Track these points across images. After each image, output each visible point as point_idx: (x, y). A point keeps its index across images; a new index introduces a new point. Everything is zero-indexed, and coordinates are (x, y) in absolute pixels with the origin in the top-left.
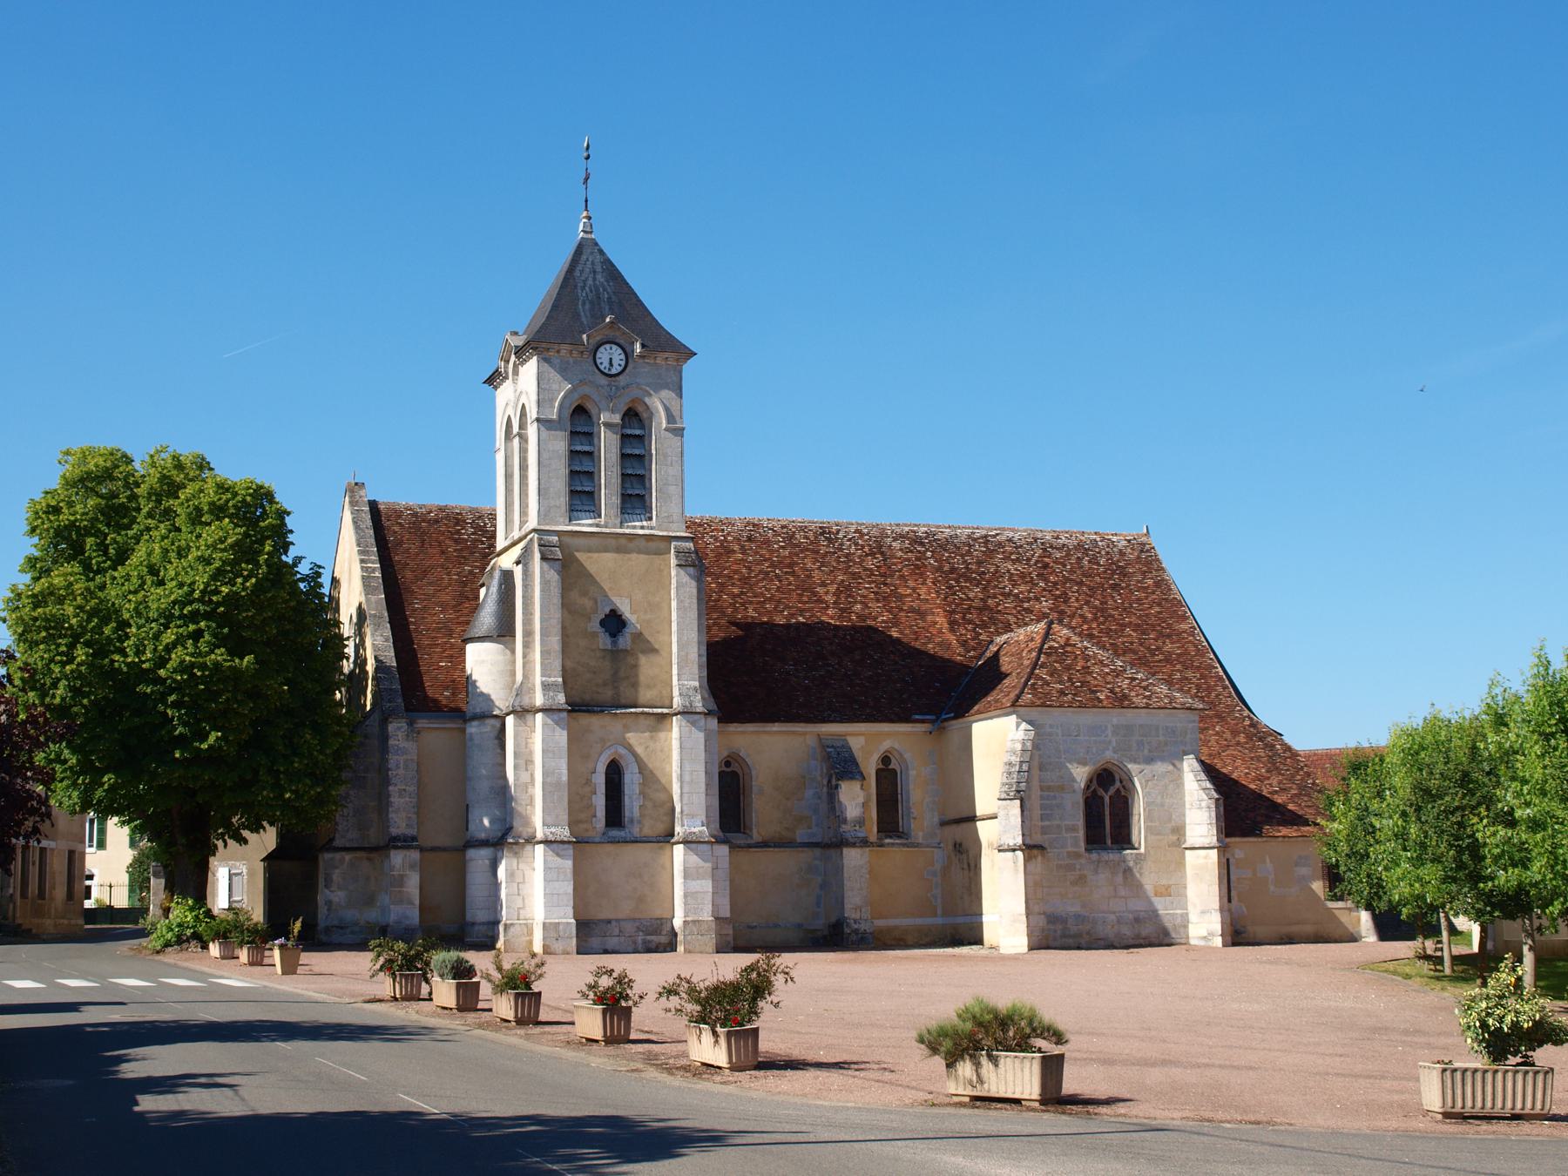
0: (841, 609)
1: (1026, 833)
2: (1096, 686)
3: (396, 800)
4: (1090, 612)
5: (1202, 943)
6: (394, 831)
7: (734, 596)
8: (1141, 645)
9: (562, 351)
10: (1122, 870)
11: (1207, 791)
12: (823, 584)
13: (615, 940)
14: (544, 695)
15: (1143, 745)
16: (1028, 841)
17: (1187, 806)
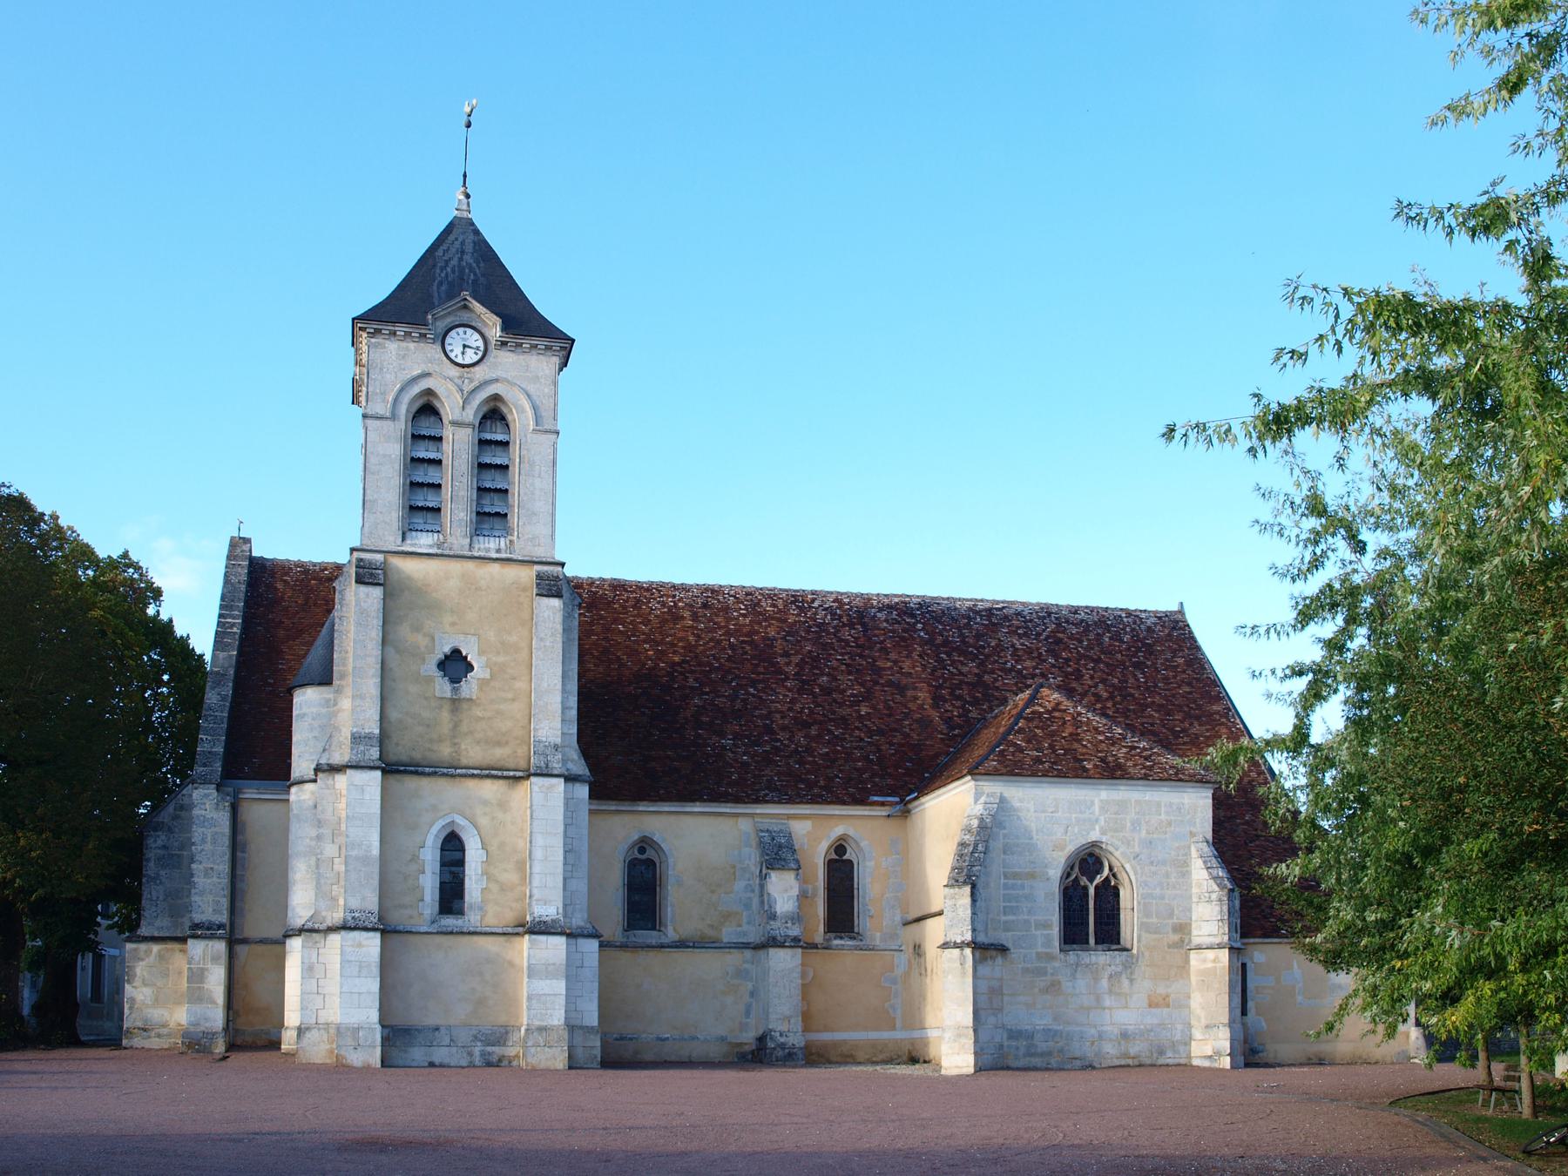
0: (803, 682)
1: (979, 927)
2: (1083, 754)
4: (1106, 691)
5: (1206, 1064)
6: (198, 918)
7: (674, 664)
8: (1164, 726)
12: (786, 654)
13: (444, 1051)
15: (1139, 824)
16: (981, 938)
17: (1195, 899)
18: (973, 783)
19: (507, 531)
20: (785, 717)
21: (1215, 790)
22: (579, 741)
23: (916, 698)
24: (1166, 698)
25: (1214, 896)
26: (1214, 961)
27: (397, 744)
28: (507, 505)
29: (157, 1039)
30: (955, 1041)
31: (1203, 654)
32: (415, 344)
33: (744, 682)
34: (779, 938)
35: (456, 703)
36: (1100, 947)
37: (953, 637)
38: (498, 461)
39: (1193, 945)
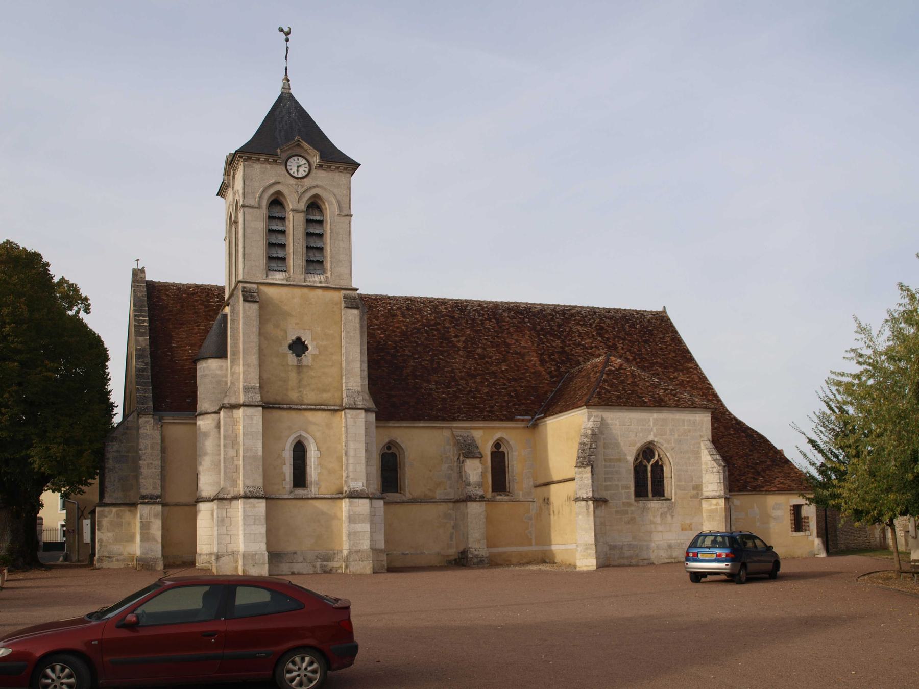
0: (468, 351)
2: (641, 394)
3: (144, 471)
4: (631, 356)
6: (144, 492)
7: (396, 342)
8: (664, 375)
9: (261, 159)
10: (659, 514)
11: (717, 461)
12: (456, 336)
14: (245, 396)
16: (596, 496)
18: (586, 410)
19: (324, 271)
20: (462, 372)
21: (712, 412)
22: (369, 389)
23: (531, 361)
24: (663, 359)
25: (715, 470)
26: (716, 505)
27: (268, 392)
28: (323, 257)
29: (117, 563)
30: (584, 551)
31: (679, 335)
32: (271, 166)
33: (436, 352)
34: (473, 496)
35: (299, 368)
36: (655, 498)
37: (546, 326)
38: (318, 232)
39: (703, 497)
